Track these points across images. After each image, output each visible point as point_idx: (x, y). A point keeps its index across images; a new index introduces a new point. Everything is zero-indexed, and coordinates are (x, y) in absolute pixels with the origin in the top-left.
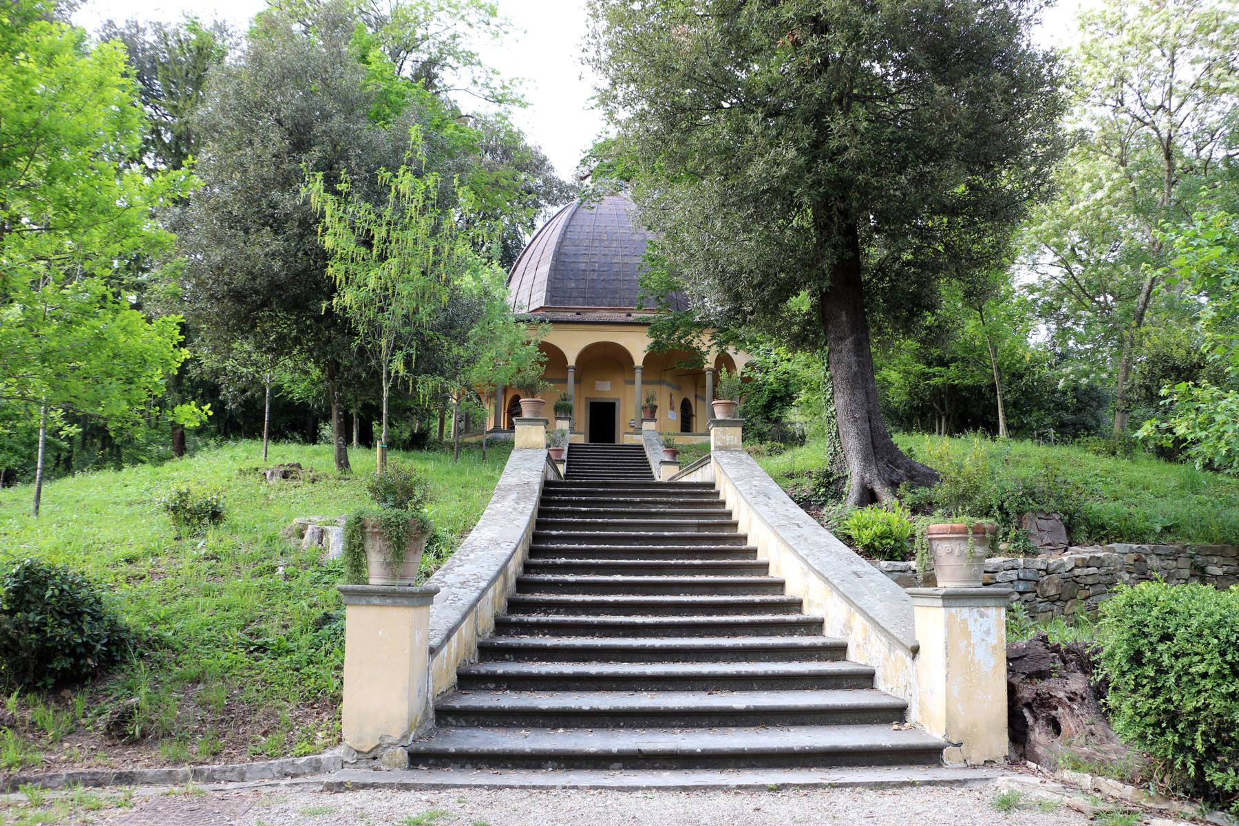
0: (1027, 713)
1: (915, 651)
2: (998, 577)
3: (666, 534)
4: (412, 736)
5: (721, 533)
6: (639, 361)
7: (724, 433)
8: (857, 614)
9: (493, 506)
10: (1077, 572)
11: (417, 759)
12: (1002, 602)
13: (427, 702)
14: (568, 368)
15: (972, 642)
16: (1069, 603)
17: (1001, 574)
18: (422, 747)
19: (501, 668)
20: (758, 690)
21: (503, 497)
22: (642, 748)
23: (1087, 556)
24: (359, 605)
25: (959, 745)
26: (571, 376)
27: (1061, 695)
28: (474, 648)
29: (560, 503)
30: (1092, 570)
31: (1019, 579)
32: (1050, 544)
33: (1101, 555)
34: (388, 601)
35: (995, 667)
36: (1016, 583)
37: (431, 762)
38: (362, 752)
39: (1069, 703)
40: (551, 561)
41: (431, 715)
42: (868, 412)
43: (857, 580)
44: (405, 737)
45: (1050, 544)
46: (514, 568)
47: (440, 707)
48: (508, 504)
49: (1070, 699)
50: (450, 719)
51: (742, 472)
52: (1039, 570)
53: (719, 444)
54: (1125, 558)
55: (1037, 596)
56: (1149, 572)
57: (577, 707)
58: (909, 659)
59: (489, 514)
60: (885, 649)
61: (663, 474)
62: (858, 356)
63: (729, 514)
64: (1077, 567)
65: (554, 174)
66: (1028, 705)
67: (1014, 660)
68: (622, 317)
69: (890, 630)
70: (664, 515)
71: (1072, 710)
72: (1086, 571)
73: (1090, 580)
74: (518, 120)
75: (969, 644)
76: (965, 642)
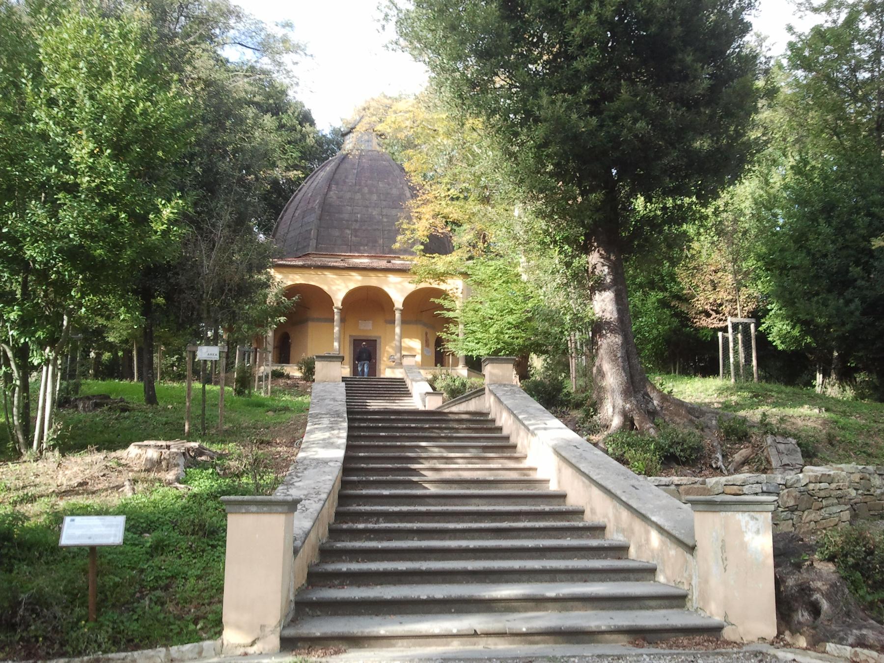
1: (691, 549)
10: (811, 486)
16: (806, 513)
17: (747, 487)
18: (291, 632)
23: (819, 474)
24: (239, 513)
29: (360, 428)
30: (823, 485)
32: (788, 465)
33: (832, 473)
34: (265, 509)
41: (293, 606)
52: (780, 484)
56: (872, 490)
57: (416, 597)
63: (507, 438)
64: (810, 482)
68: (383, 264)
72: (818, 485)
73: (822, 494)
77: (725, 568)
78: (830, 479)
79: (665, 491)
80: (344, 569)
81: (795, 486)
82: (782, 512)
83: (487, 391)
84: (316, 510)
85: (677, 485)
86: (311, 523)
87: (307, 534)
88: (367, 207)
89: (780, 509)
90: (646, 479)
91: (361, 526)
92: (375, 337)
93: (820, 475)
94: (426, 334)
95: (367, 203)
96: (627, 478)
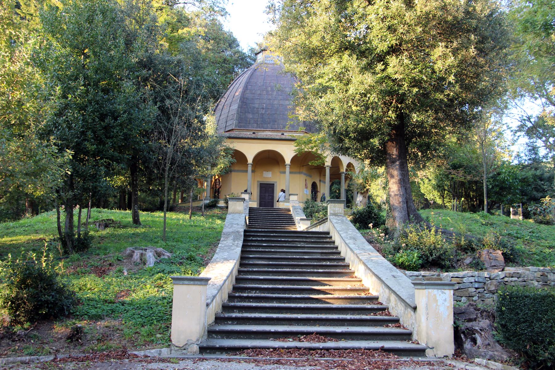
0: (462, 336)
1: (415, 309)
5: (245, 286)
6: (288, 161)
7: (335, 207)
9: (222, 243)
10: (506, 279)
11: (203, 350)
12: (451, 287)
14: (248, 164)
15: (438, 304)
17: (465, 279)
21: (227, 238)
23: (512, 272)
26: (250, 168)
27: (477, 328)
28: (221, 306)
29: (252, 241)
30: (514, 279)
31: (475, 282)
32: (495, 266)
35: (448, 315)
36: (473, 283)
37: (208, 351)
38: (180, 347)
39: (480, 332)
40: (251, 269)
41: (206, 333)
42: (406, 198)
44: (198, 340)
45: (495, 266)
46: (235, 273)
48: (229, 242)
49: (481, 330)
50: (214, 335)
51: (343, 227)
52: (486, 278)
53: (332, 212)
54: (536, 274)
55: (485, 290)
56: (549, 282)
58: (412, 313)
59: (221, 246)
60: (403, 309)
61: (301, 226)
62: (402, 171)
63: (337, 248)
64: (506, 277)
65: (240, 49)
66: (463, 333)
67: (458, 314)
68: (277, 135)
69: (405, 300)
71: (481, 335)
72: (511, 279)
75: (437, 305)
76: (435, 304)
77: (427, 319)
78: (519, 276)
81: (496, 278)
82: (486, 293)
85: (423, 276)
86: (217, 291)
87: (214, 297)
88: (270, 99)
89: (485, 292)
92: (273, 182)
93: (512, 273)
95: (270, 97)
96: (391, 271)
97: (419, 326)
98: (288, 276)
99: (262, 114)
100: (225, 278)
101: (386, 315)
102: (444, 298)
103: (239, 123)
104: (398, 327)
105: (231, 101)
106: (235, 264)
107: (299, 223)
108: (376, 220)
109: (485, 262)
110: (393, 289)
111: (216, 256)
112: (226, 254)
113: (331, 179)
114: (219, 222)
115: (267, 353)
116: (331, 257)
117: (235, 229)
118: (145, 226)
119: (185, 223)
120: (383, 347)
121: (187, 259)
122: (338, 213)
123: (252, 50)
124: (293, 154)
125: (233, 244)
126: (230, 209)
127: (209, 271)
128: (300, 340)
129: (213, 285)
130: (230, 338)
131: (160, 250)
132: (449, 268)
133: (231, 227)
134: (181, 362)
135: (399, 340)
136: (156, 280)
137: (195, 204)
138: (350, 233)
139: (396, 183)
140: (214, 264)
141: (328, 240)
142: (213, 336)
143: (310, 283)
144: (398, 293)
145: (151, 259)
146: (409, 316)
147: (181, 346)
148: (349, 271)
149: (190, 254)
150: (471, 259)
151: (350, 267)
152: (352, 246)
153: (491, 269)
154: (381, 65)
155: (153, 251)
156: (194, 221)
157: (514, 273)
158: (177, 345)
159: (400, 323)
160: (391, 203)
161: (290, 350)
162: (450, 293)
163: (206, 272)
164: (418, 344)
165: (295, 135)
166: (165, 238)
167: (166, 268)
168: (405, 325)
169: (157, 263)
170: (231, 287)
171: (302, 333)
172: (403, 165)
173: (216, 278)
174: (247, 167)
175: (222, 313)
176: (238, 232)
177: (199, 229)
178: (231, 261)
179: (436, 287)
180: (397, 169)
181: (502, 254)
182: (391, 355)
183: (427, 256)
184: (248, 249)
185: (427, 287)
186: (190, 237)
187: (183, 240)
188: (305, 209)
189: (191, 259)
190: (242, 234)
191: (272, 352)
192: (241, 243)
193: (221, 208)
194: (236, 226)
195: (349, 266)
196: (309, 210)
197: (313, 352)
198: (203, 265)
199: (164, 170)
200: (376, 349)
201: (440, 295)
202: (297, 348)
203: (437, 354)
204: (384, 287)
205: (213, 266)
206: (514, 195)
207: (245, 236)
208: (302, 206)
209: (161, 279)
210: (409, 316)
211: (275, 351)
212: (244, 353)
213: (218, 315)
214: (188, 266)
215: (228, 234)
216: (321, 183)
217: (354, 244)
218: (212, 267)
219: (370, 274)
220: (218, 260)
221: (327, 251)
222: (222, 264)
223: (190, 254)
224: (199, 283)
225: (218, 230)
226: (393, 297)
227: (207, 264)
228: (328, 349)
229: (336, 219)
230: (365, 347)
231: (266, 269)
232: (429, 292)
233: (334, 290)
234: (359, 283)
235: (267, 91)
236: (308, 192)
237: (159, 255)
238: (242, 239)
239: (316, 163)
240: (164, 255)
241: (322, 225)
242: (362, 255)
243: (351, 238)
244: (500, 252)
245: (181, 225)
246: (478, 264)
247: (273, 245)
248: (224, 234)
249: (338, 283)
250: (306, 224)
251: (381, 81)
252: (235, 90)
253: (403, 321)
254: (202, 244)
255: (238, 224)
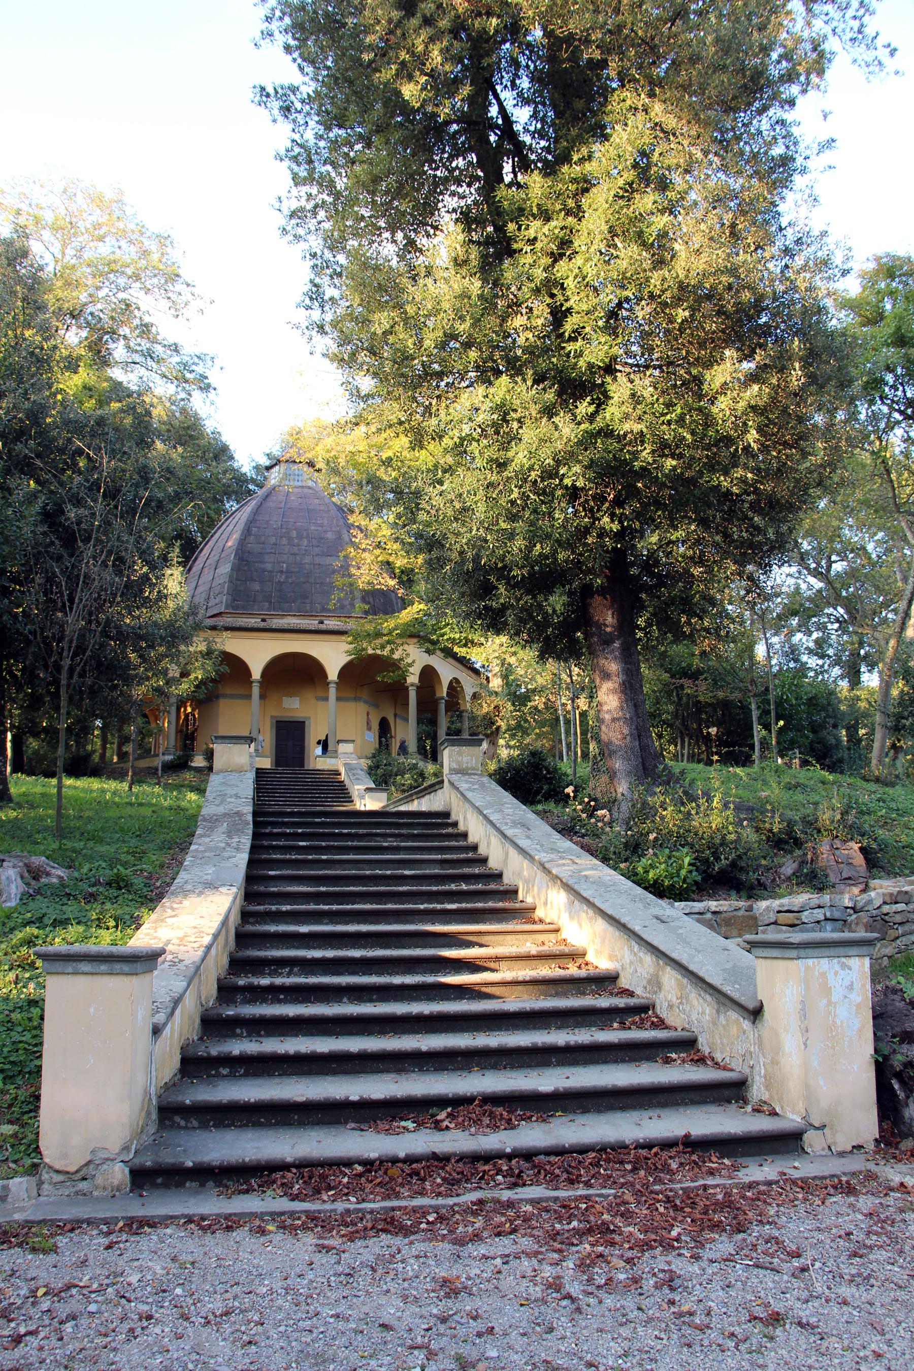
1: (756, 1013)
2: (805, 916)
3: (407, 872)
4: (134, 1147)
6: (333, 674)
7: (460, 754)
8: (668, 969)
9: (200, 841)
10: (886, 909)
12: (864, 950)
13: (150, 1099)
15: (833, 1000)
17: (806, 913)
19: (239, 1047)
20: (558, 1065)
21: (212, 829)
22: (437, 1151)
25: (822, 1127)
26: (256, 690)
28: (198, 1021)
29: (272, 836)
30: (901, 907)
31: (826, 919)
32: (849, 878)
36: (823, 923)
37: (159, 1180)
38: (68, 1173)
40: (274, 908)
41: (154, 1116)
42: (637, 728)
43: (662, 926)
44: (126, 1148)
45: (849, 878)
46: (234, 919)
47: (164, 1103)
48: (218, 838)
50: (177, 1119)
51: (488, 798)
52: (847, 908)
53: (454, 766)
57: (343, 1098)
59: (196, 850)
62: (626, 663)
63: (475, 848)
64: (885, 903)
65: (236, 465)
66: (899, 1076)
68: (313, 624)
69: (720, 987)
70: (397, 849)
73: (898, 918)
74: (198, 403)
75: (830, 1003)
76: (825, 1001)
77: (805, 1044)
79: (698, 921)
80: (236, 1052)
83: (446, 783)
84: (194, 963)
85: (714, 913)
86: (185, 984)
87: (177, 1002)
88: (294, 554)
90: (673, 906)
91: (265, 981)
94: (368, 714)
95: (296, 549)
96: (647, 905)
97: (775, 1062)
98: (371, 923)
99: (280, 583)
100: (207, 940)
101: (654, 1026)
102: (846, 983)
103: (234, 600)
104: (698, 1061)
105: (216, 558)
106: (235, 898)
107: (362, 797)
108: (551, 783)
109: (828, 871)
110: (675, 955)
111: (183, 876)
112: (211, 870)
113: (420, 711)
114: (193, 796)
115: (346, 1180)
116: (467, 870)
117: (230, 806)
118: (20, 806)
119: (117, 799)
120: (687, 1136)
121: (109, 884)
122: (467, 768)
123: (257, 468)
124: (344, 659)
125: (228, 844)
126: (218, 763)
127: (162, 921)
128: (437, 1126)
129: (173, 964)
130: (228, 1126)
131: (39, 860)
132: (752, 888)
133: (221, 803)
134: (62, 1241)
135: (711, 1102)
136: (15, 950)
137: (143, 764)
138: (510, 811)
139: (614, 691)
140: (176, 900)
141: (450, 830)
142: (174, 1122)
143: (430, 940)
144: (692, 967)
145: (13, 886)
146: (734, 1030)
147: (72, 1169)
148: (518, 905)
149: (115, 871)
150: (795, 865)
151: (520, 896)
152: (524, 843)
153: (843, 887)
154: (585, 404)
155: (21, 864)
156: (137, 796)
157: (899, 892)
158: (57, 1167)
159: (698, 1051)
160: (604, 737)
161: (414, 1166)
162: (863, 965)
163: (156, 921)
164: (774, 1113)
165: (351, 625)
166: (61, 831)
167: (50, 911)
168: (718, 1057)
169: (27, 897)
170: (225, 961)
171: (441, 1102)
172: (628, 649)
173: (181, 939)
174: (251, 687)
175: (201, 1039)
176: (238, 814)
177: (147, 811)
178: (224, 890)
179: (827, 952)
180: (616, 657)
181: (862, 849)
182: (714, 1159)
183: (706, 861)
184: (264, 856)
185: (802, 952)
186: (122, 830)
187: (105, 835)
188: (372, 771)
189: (119, 884)
190: (250, 818)
191: (360, 1175)
192: (246, 841)
193: (198, 770)
194: (232, 800)
195: (516, 892)
196: (380, 771)
197: (486, 1168)
198: (151, 900)
199: (58, 668)
200: (667, 1145)
201: (836, 973)
202: (435, 1156)
203: (835, 1143)
204: (636, 948)
205: (175, 906)
206: (798, 730)
207: (255, 823)
208: (364, 763)
209: (30, 943)
210: (734, 1030)
211: (370, 1171)
212: (274, 1182)
213: (191, 1052)
214: (108, 906)
215: (214, 821)
216: (398, 720)
217: (528, 837)
218: (173, 909)
219: (586, 914)
220: (189, 887)
221: (455, 857)
222: (199, 899)
223: (115, 871)
224: (126, 968)
225: (191, 812)
226: (670, 978)
227: (161, 896)
228: (528, 1155)
229: (467, 782)
230: (637, 1141)
231: (312, 907)
232: (807, 968)
233: (498, 959)
234: (552, 937)
235: (290, 539)
236: (372, 738)
237: (35, 874)
238: (250, 832)
239: (388, 677)
240: (48, 874)
241: (427, 797)
242: (559, 866)
243: (515, 824)
244: (856, 847)
245: (107, 802)
246: (815, 877)
247: (323, 844)
248: (205, 820)
249: (499, 938)
250: (379, 800)
251: (587, 441)
252: (225, 536)
253: (712, 1045)
254: (151, 846)
255: (237, 796)
